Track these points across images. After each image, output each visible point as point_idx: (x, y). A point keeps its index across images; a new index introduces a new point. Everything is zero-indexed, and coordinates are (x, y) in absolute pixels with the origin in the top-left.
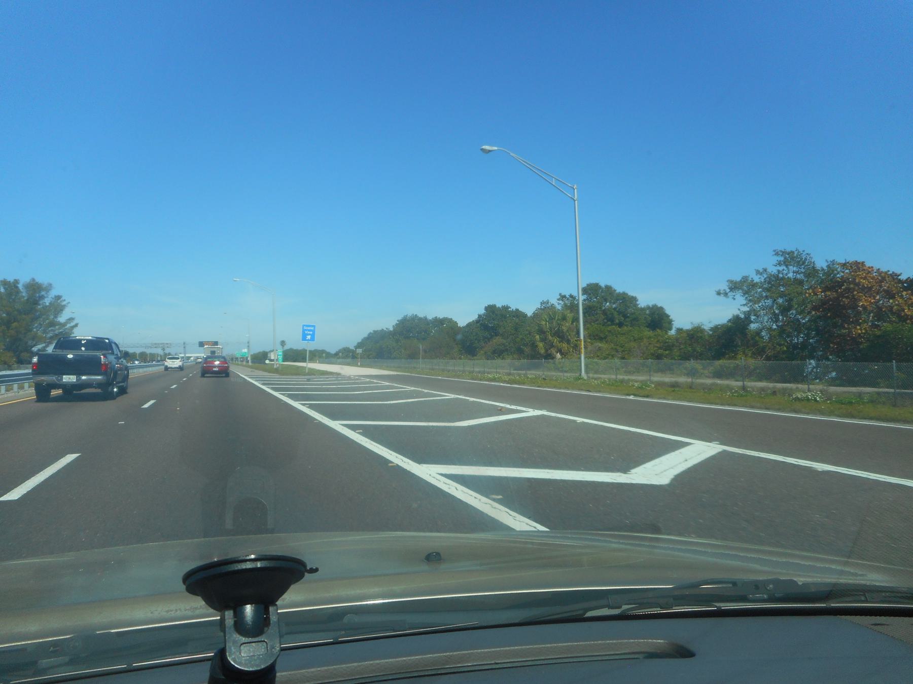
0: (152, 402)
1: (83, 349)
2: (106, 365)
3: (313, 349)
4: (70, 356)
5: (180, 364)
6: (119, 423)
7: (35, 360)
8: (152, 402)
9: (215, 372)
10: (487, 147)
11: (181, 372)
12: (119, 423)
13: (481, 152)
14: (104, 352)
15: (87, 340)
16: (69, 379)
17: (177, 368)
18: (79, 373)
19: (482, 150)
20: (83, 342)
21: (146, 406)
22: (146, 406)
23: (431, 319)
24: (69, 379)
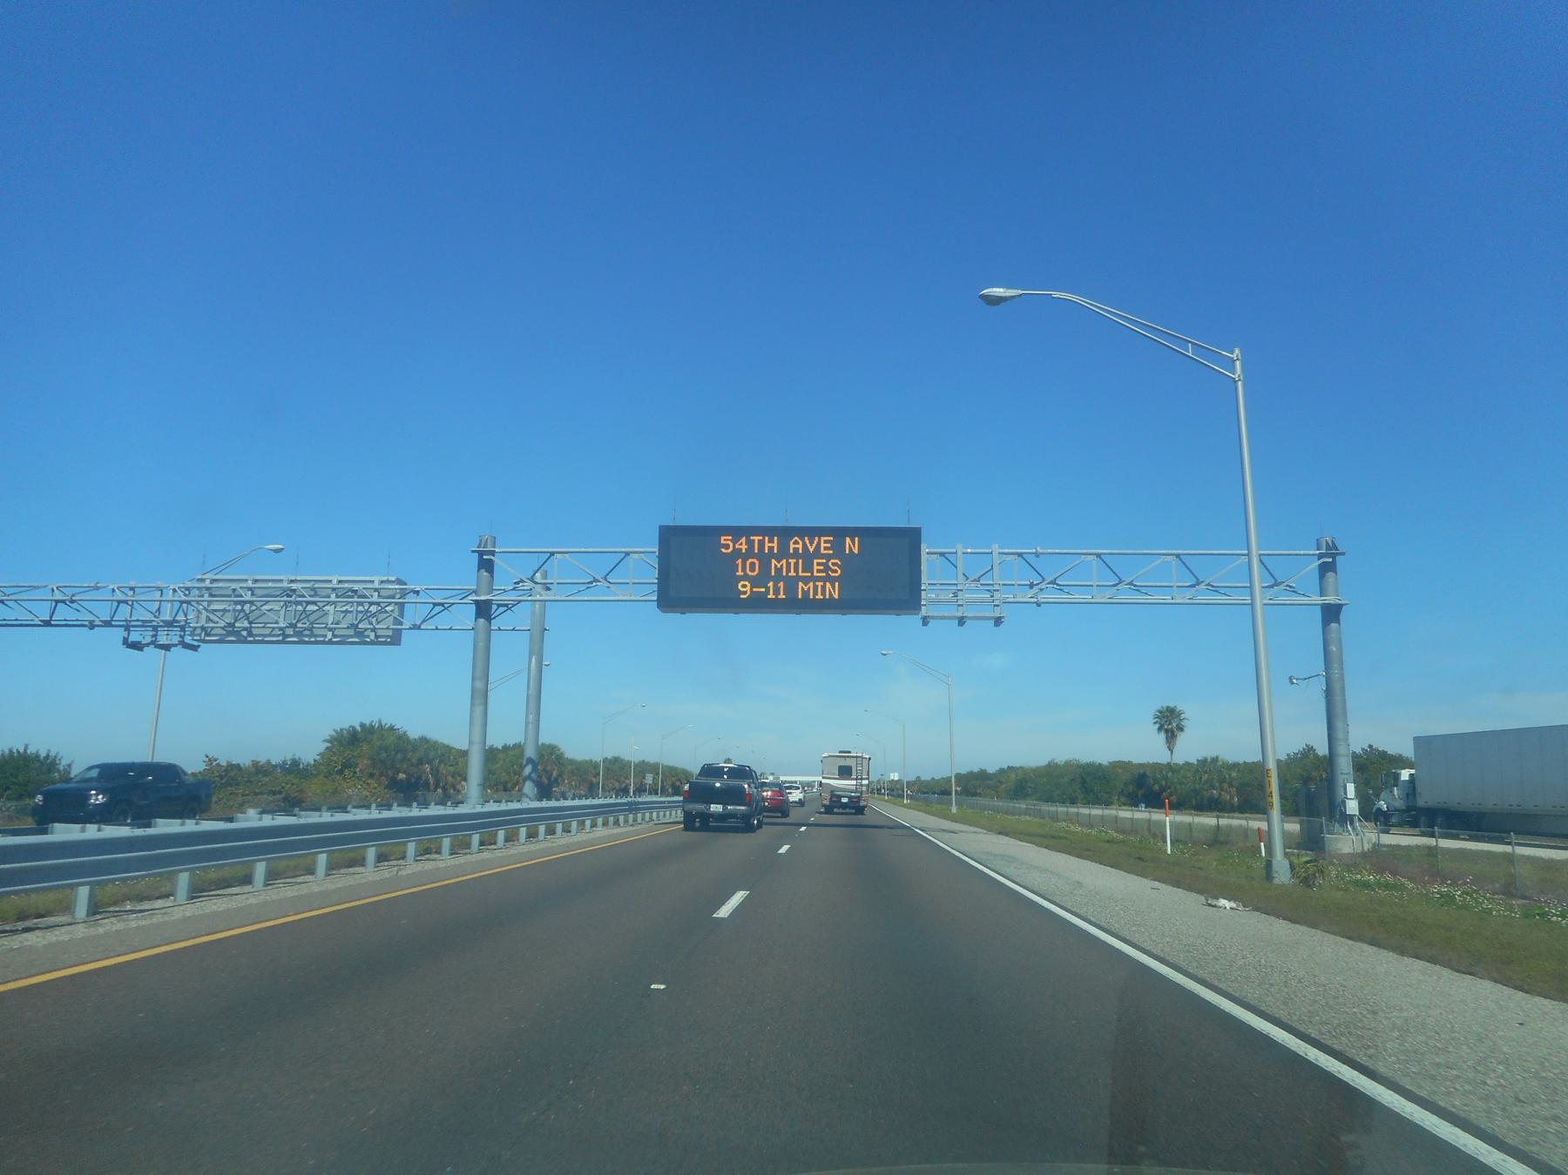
0: (739, 897)
1: (725, 777)
2: (749, 794)
3: (964, 771)
4: (718, 785)
5: (801, 796)
6: (662, 987)
7: (686, 787)
8: (739, 897)
9: (844, 806)
10: (999, 291)
11: (802, 808)
12: (662, 987)
13: (980, 301)
14: (748, 781)
15: (729, 768)
16: (716, 808)
17: (796, 802)
18: (724, 804)
19: (983, 297)
20: (726, 770)
21: (724, 912)
22: (724, 912)
23: (416, 737)
24: (716, 808)
